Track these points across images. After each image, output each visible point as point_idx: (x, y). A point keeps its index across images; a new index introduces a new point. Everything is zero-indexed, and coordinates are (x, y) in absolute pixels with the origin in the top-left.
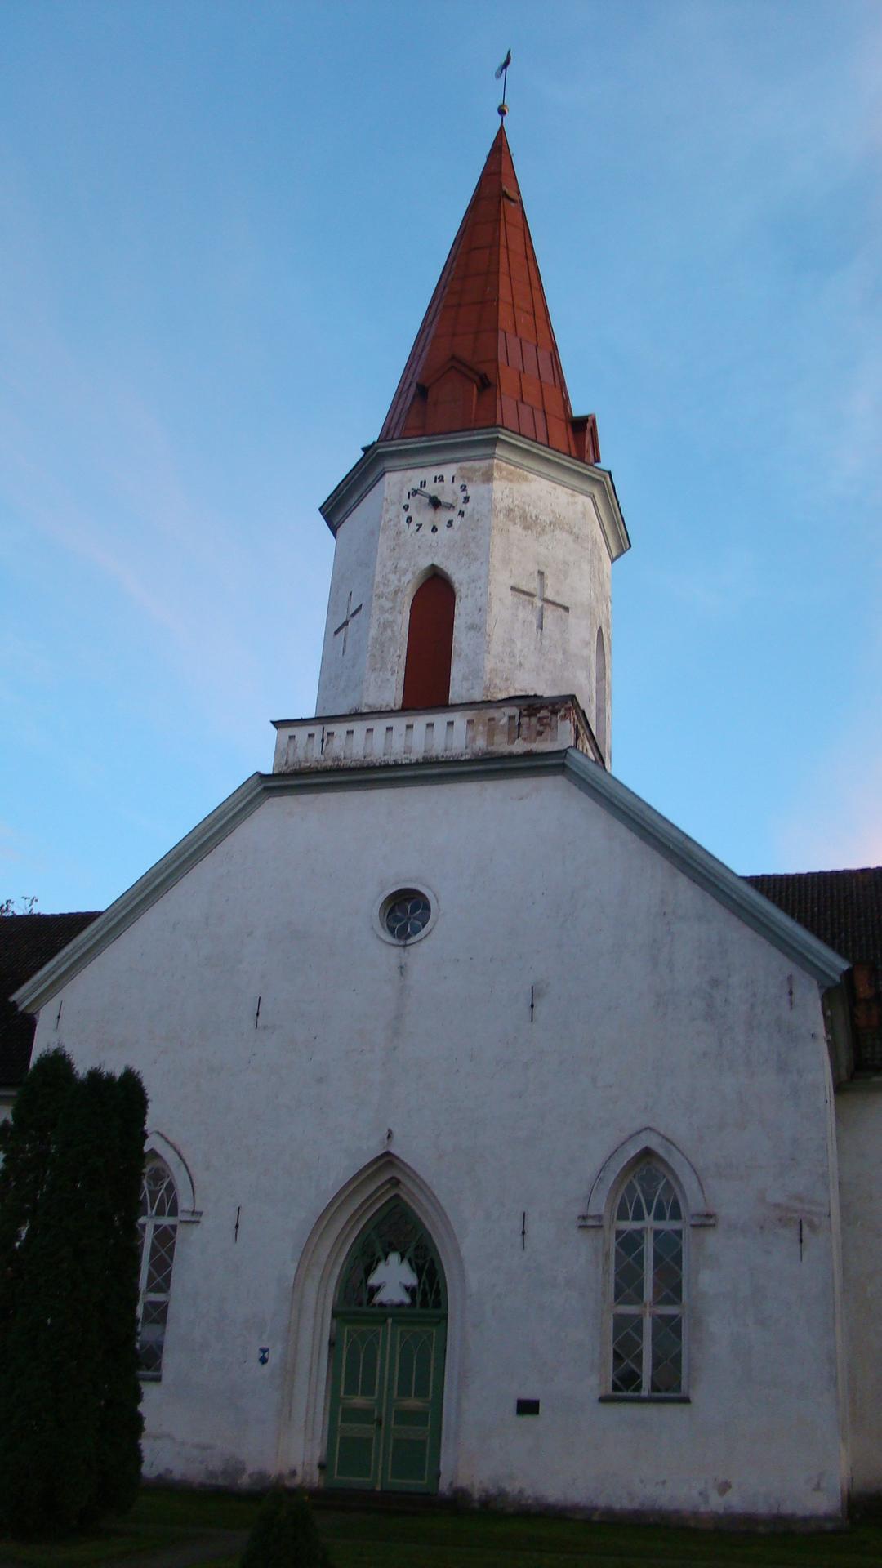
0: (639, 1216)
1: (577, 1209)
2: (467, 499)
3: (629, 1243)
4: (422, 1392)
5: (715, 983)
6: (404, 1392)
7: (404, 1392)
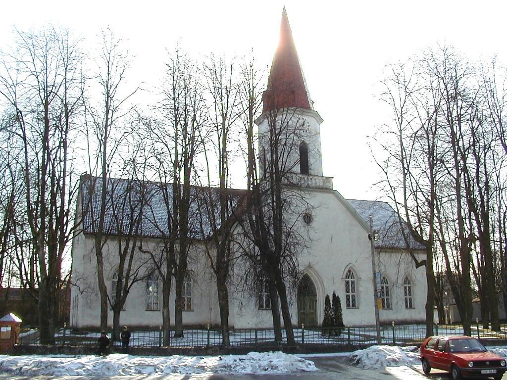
0: (348, 278)
1: (342, 277)
2: (309, 126)
3: (347, 283)
4: (313, 309)
5: (359, 238)
6: (310, 309)
7: (310, 309)
